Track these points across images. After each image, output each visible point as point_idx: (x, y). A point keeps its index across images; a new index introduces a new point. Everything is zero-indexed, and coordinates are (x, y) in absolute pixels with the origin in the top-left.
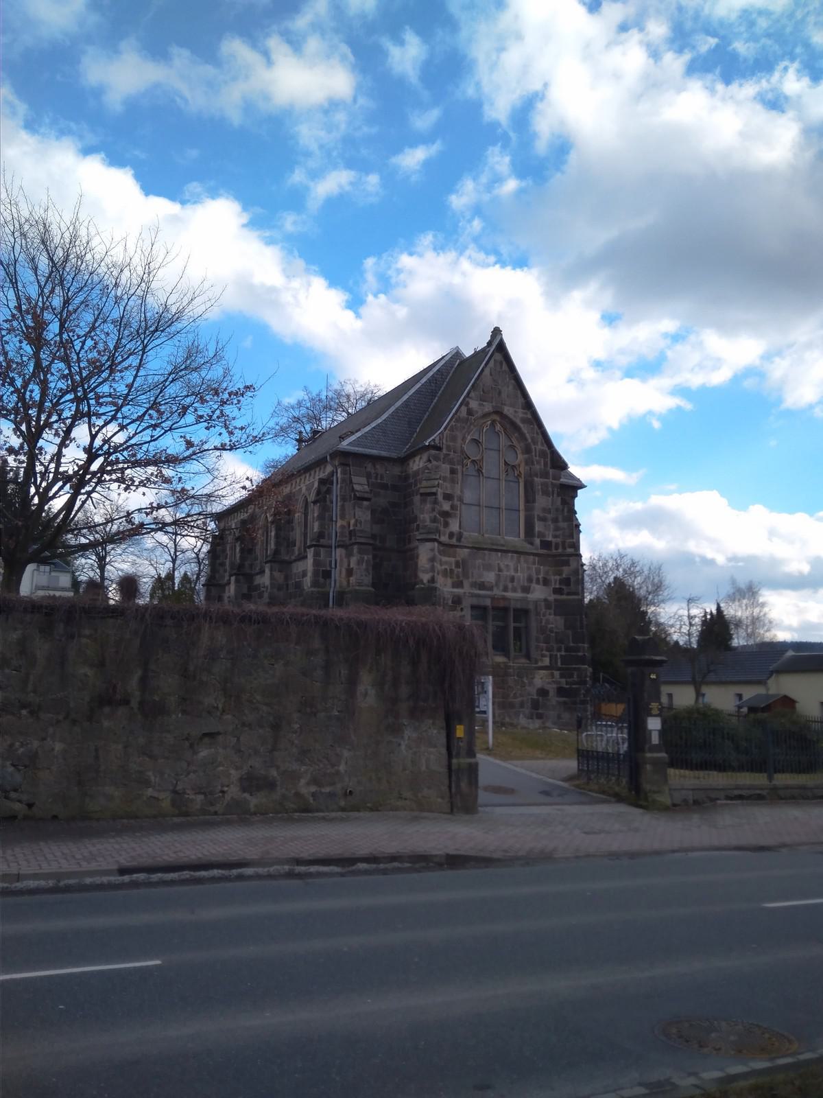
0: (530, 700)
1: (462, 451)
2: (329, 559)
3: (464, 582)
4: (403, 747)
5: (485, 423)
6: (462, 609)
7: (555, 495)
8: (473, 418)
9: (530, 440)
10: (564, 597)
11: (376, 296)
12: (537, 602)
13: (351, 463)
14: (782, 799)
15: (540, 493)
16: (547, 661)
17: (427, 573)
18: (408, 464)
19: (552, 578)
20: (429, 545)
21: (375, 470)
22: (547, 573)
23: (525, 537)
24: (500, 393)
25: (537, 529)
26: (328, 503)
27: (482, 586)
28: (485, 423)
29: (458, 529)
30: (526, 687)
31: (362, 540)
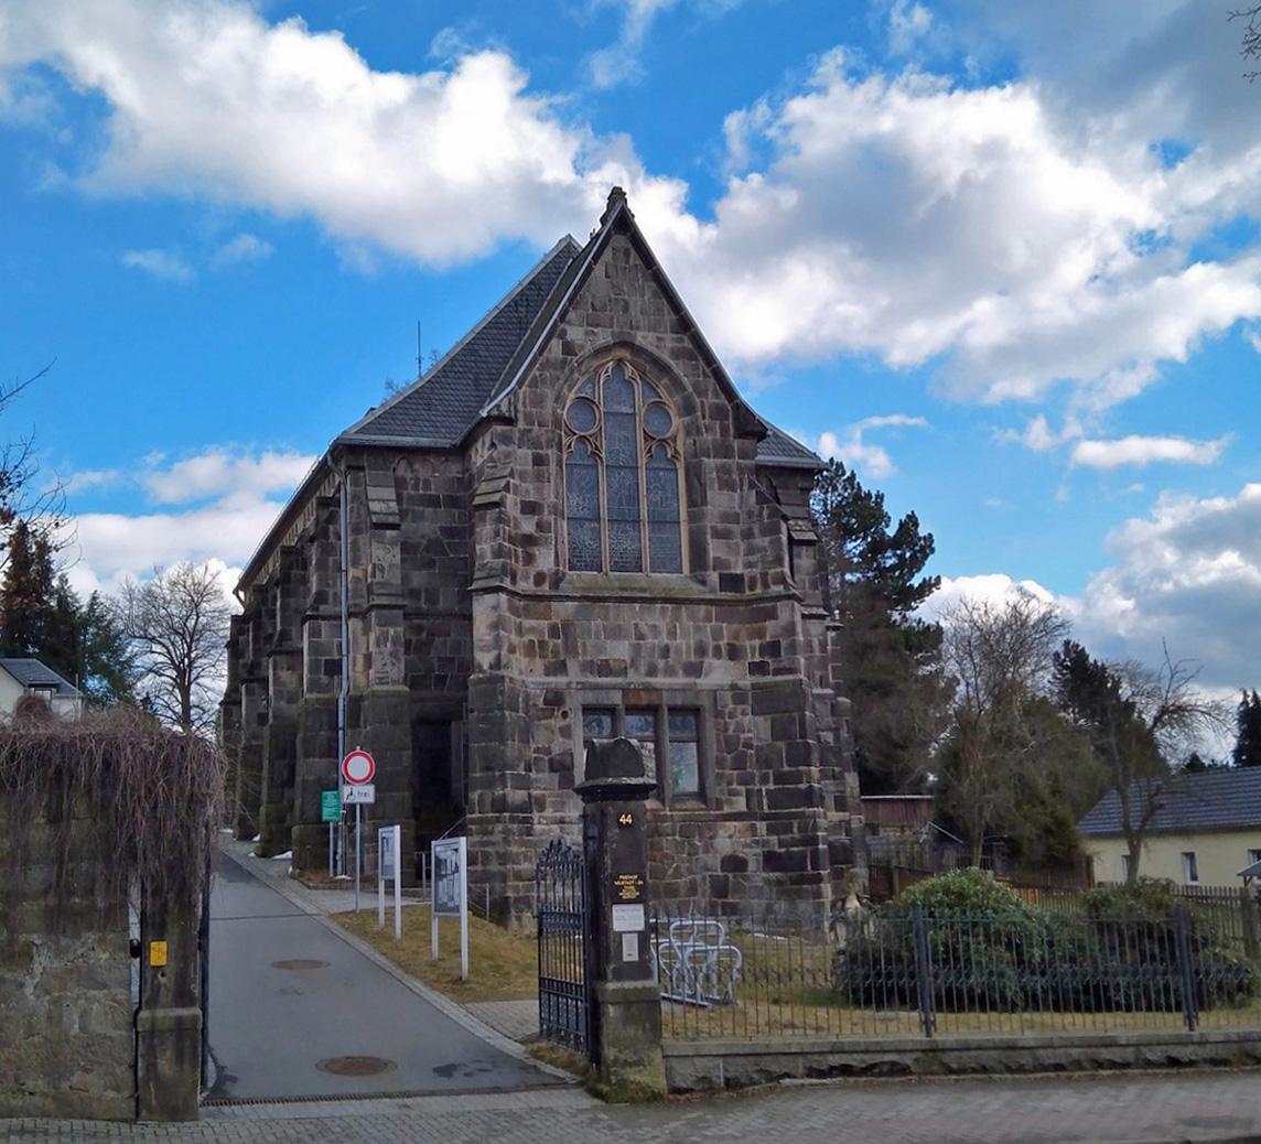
0: (708, 879)
1: (557, 422)
2: (336, 640)
3: (568, 662)
4: (29, 990)
5: (603, 365)
6: (565, 715)
7: (745, 488)
8: (575, 359)
9: (690, 389)
10: (769, 678)
11: (743, 176)
12: (715, 691)
13: (366, 464)
14: (951, 1071)
15: (716, 486)
16: (741, 804)
17: (489, 651)
18: (470, 457)
19: (747, 643)
20: (489, 599)
21: (412, 471)
22: (736, 635)
23: (691, 572)
24: (626, 309)
25: (711, 554)
26: (332, 539)
27: (604, 668)
28: (603, 365)
29: (552, 565)
30: (701, 855)
31: (384, 601)
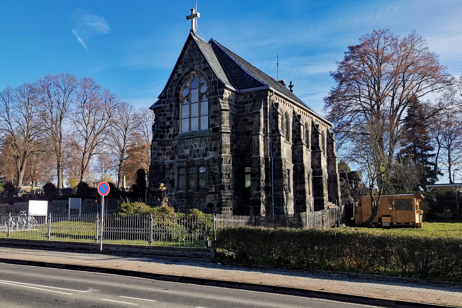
6: (173, 169)
27: (184, 157)
